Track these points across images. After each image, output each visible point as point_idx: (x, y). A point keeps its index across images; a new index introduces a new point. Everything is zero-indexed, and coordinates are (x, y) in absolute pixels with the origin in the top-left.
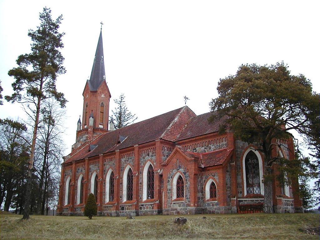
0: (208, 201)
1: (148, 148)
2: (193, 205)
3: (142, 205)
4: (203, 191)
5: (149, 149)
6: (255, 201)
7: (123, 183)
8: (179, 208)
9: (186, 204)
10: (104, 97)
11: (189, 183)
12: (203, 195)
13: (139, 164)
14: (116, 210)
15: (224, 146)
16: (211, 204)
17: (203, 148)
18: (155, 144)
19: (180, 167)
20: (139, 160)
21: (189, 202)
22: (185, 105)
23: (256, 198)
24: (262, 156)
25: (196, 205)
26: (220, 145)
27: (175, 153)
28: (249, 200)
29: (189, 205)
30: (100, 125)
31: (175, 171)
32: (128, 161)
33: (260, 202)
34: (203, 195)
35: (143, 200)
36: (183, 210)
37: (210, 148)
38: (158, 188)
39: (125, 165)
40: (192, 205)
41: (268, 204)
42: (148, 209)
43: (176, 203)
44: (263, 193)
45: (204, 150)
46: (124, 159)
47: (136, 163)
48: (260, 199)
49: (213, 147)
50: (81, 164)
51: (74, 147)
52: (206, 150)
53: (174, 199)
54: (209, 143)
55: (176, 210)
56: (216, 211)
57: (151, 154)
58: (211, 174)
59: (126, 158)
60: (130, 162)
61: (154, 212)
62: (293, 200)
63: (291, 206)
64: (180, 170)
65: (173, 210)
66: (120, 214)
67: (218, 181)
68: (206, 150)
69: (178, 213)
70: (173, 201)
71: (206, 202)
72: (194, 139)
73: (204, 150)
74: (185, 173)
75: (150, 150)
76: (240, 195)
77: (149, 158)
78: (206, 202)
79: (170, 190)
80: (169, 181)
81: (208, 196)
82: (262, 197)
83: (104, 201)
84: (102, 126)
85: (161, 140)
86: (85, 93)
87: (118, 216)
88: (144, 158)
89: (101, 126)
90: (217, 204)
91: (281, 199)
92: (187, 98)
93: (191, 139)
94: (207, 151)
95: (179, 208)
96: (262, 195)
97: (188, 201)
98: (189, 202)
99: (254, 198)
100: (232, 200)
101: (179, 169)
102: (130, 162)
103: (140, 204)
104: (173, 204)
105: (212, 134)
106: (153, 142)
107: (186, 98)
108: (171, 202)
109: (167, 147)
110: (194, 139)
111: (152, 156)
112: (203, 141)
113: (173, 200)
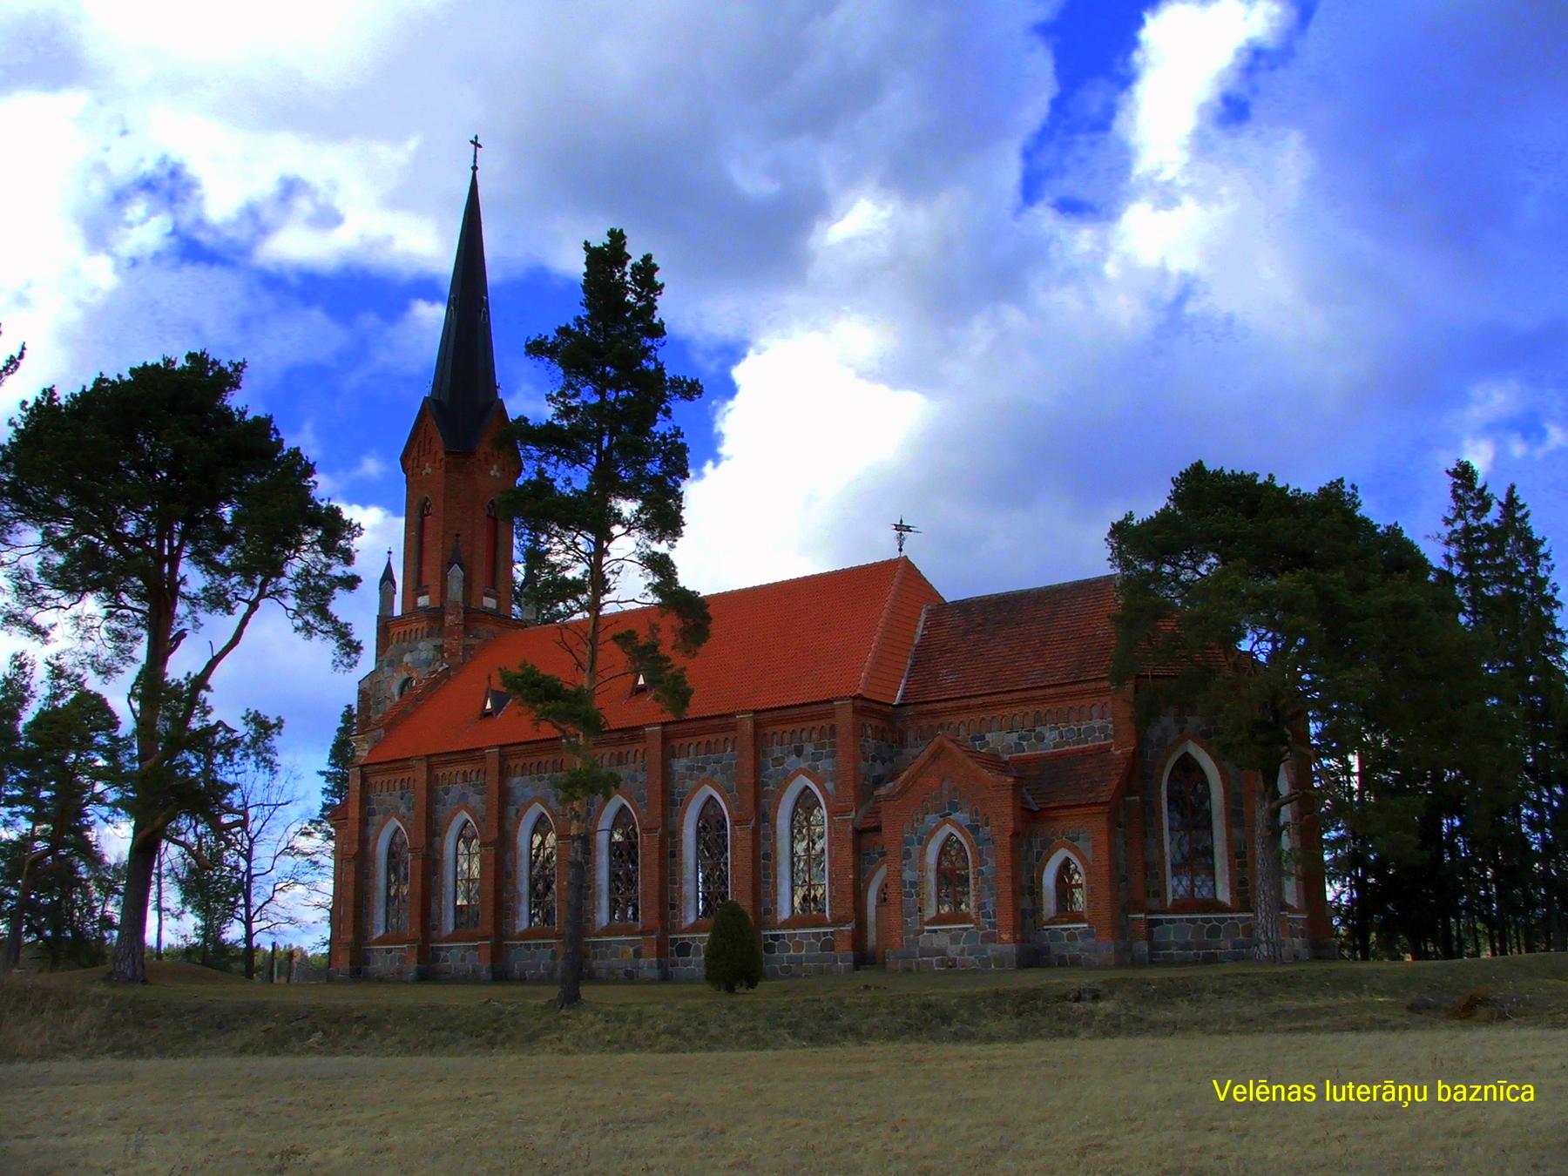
0: (1052, 921)
1: (797, 727)
2: (1008, 935)
3: (775, 937)
4: (1034, 889)
5: (803, 730)
6: (1199, 923)
7: (684, 852)
8: (952, 950)
9: (981, 932)
10: (498, 475)
11: (991, 863)
12: (1034, 904)
13: (758, 785)
14: (658, 957)
15: (1097, 734)
16: (1065, 934)
17: (1014, 736)
18: (831, 715)
19: (955, 807)
20: (758, 769)
21: (993, 925)
22: (896, 555)
23: (1205, 912)
24: (1222, 771)
25: (1018, 936)
26: (1079, 729)
27: (935, 756)
28: (1181, 920)
29: (990, 938)
30: (485, 599)
31: (931, 819)
32: (703, 769)
33: (1215, 925)
34: (1034, 904)
35: (778, 918)
36: (970, 954)
37: (1041, 738)
38: (851, 876)
39: (690, 784)
40: (1005, 937)
41: (1269, 934)
42: (804, 952)
43: (940, 930)
44: (1224, 895)
45: (1016, 744)
46: (684, 761)
47: (749, 779)
48: (1188, 917)
49: (1051, 736)
50: (461, 768)
51: (367, 685)
52: (1024, 743)
53: (931, 916)
54: (1039, 720)
55: (942, 952)
56: (1083, 957)
57: (809, 749)
58: (1063, 833)
59: (692, 756)
60: (714, 773)
61: (839, 963)
62: (1305, 917)
63: (1301, 938)
64: (957, 816)
65: (926, 952)
66: (670, 969)
67: (1089, 857)
68: (1024, 743)
69: (951, 965)
70: (928, 924)
71: (1046, 927)
72: (980, 701)
73: (1016, 744)
74: (974, 829)
75: (805, 735)
76: (1153, 903)
77: (804, 765)
78: (1046, 927)
79: (913, 884)
80: (908, 854)
81: (1049, 906)
82: (1221, 908)
83: (591, 921)
84: (494, 601)
85: (859, 703)
86: (415, 454)
87: (665, 978)
88: (778, 762)
89: (489, 603)
90: (1086, 934)
91: (1285, 915)
92: (908, 529)
93: (964, 702)
94: (1029, 746)
95: (954, 947)
96: (1219, 902)
97: (990, 922)
98: (993, 925)
99: (1199, 912)
100: (1133, 919)
101: (950, 814)
102: (714, 773)
103: (768, 933)
104: (925, 934)
105: (1052, 691)
106: (828, 706)
107: (901, 528)
108: (918, 928)
109: (874, 727)
110: (980, 701)
111: (816, 757)
112: (1015, 711)
113: (926, 919)
